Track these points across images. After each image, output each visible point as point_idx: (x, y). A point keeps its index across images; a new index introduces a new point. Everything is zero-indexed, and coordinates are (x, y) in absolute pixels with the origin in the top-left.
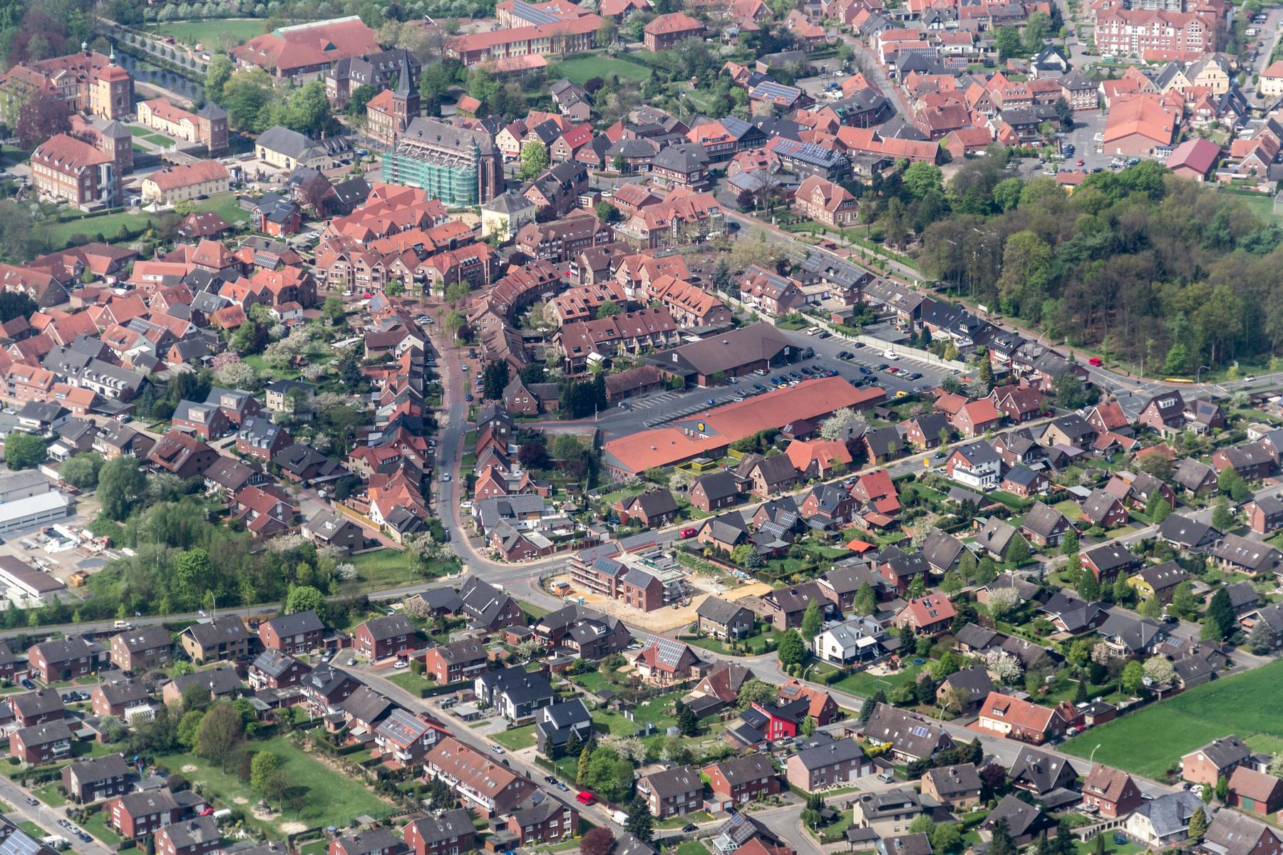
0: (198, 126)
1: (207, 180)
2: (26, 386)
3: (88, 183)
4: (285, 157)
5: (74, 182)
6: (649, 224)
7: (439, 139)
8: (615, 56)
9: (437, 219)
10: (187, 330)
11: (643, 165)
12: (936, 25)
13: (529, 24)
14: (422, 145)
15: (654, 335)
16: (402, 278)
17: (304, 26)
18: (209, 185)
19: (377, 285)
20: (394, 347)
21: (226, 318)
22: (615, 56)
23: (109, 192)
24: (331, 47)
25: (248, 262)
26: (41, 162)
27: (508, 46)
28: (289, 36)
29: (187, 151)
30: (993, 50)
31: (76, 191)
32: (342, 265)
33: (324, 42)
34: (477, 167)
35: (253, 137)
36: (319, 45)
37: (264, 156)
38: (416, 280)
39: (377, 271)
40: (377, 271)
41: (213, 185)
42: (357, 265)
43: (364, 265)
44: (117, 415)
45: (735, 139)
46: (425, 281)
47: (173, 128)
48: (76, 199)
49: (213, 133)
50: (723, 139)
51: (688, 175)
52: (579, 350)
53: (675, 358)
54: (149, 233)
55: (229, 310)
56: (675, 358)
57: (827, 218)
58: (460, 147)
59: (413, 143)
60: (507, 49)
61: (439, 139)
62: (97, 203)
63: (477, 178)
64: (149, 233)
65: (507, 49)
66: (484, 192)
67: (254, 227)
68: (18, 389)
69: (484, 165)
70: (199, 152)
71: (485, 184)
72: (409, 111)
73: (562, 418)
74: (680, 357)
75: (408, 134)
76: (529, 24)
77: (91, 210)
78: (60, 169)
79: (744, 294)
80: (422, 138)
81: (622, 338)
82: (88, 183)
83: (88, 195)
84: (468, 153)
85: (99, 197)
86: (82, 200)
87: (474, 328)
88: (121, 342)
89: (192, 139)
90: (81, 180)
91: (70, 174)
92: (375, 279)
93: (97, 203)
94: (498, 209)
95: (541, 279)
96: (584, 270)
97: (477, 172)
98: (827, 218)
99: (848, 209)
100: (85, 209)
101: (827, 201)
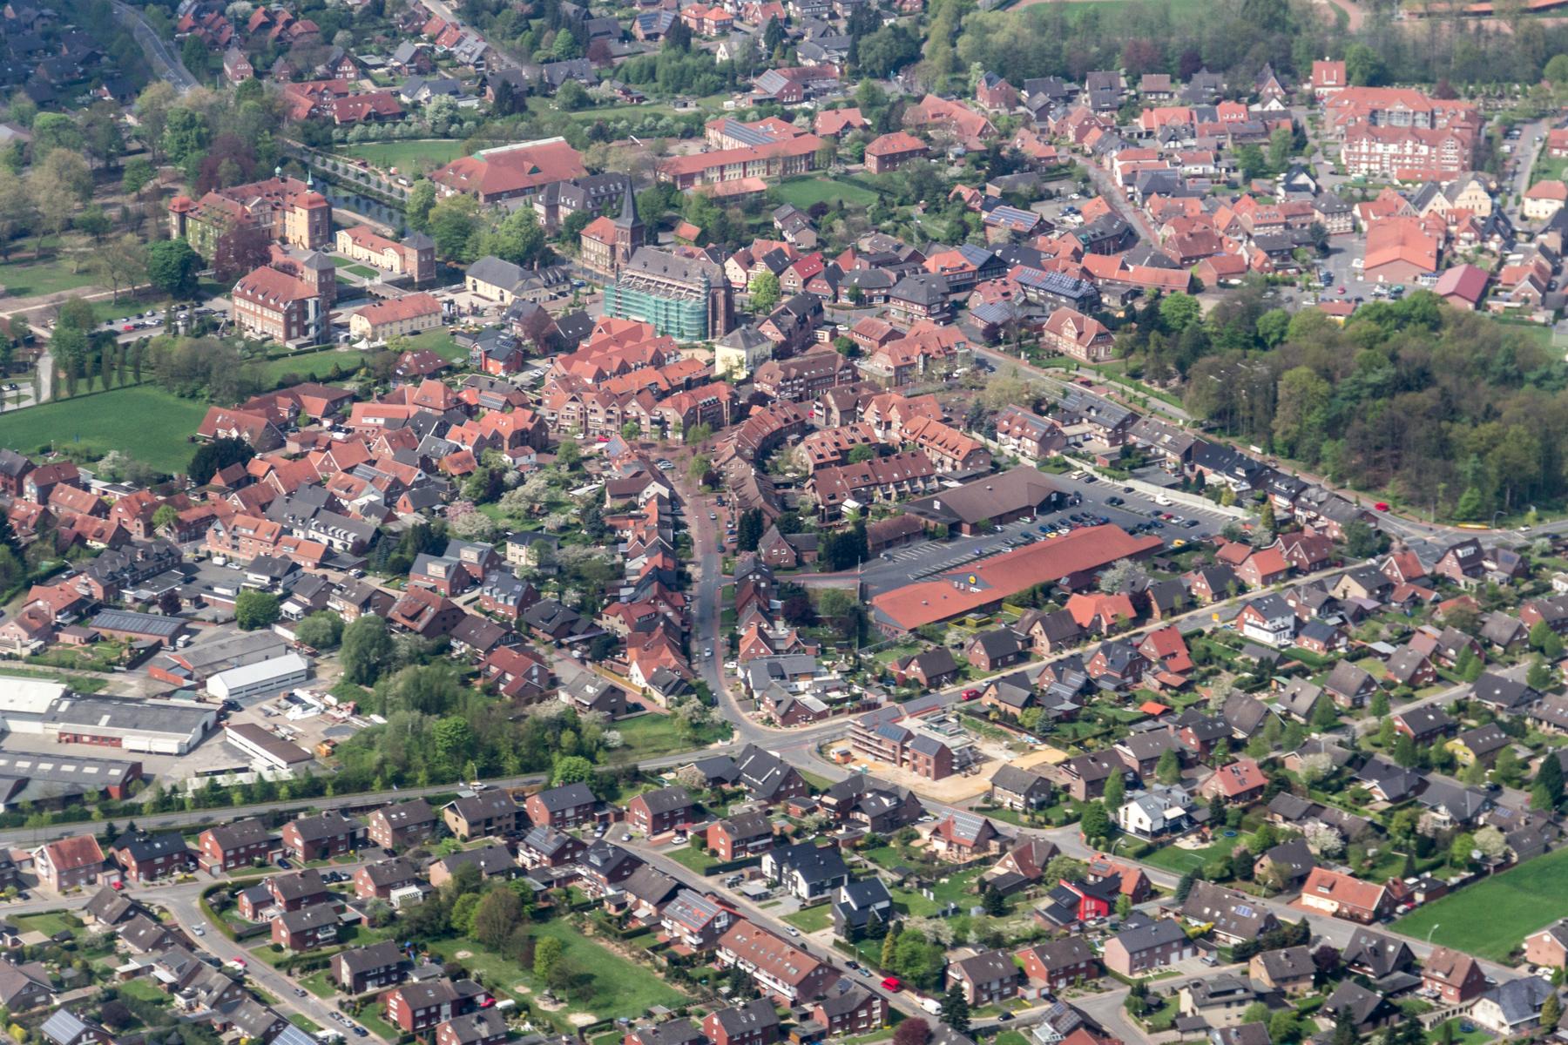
0: (403, 256)
1: (420, 315)
2: (251, 538)
3: (294, 318)
5: (280, 318)
6: (894, 361)
8: (835, 178)
10: (415, 478)
11: (879, 297)
12: (1172, 144)
13: (743, 145)
15: (912, 481)
16: (638, 420)
17: (517, 147)
18: (421, 320)
19: (611, 427)
20: (637, 495)
21: (456, 463)
22: (835, 178)
23: (317, 328)
24: (535, 170)
25: (473, 403)
26: (243, 296)
27: (722, 168)
28: (490, 158)
29: (391, 283)
30: (1235, 170)
31: (282, 327)
32: (573, 406)
33: (528, 166)
35: (461, 267)
36: (523, 168)
37: (475, 288)
38: (653, 422)
39: (610, 412)
40: (610, 412)
41: (425, 319)
42: (591, 406)
43: (597, 406)
44: (349, 569)
45: (975, 268)
46: (662, 423)
47: (376, 258)
48: (281, 335)
49: (420, 264)
50: (962, 268)
51: (929, 307)
52: (833, 497)
53: (937, 505)
54: (363, 371)
55: (458, 455)
56: (937, 505)
57: (1080, 353)
58: (688, 279)
62: (304, 340)
64: (363, 371)
66: (714, 326)
67: (474, 365)
68: (242, 542)
70: (405, 284)
71: (715, 318)
73: (822, 571)
74: (942, 505)
75: (631, 265)
76: (743, 145)
77: (298, 347)
78: (265, 304)
79: (999, 435)
81: (878, 484)
82: (294, 318)
83: (294, 331)
84: (697, 285)
85: (306, 334)
86: (288, 337)
87: (720, 474)
88: (348, 490)
89: (397, 270)
90: (288, 315)
91: (275, 309)
92: (609, 421)
93: (304, 340)
94: (733, 345)
95: (786, 420)
96: (829, 410)
98: (1080, 353)
99: (1102, 343)
100: (291, 346)
101: (1080, 334)
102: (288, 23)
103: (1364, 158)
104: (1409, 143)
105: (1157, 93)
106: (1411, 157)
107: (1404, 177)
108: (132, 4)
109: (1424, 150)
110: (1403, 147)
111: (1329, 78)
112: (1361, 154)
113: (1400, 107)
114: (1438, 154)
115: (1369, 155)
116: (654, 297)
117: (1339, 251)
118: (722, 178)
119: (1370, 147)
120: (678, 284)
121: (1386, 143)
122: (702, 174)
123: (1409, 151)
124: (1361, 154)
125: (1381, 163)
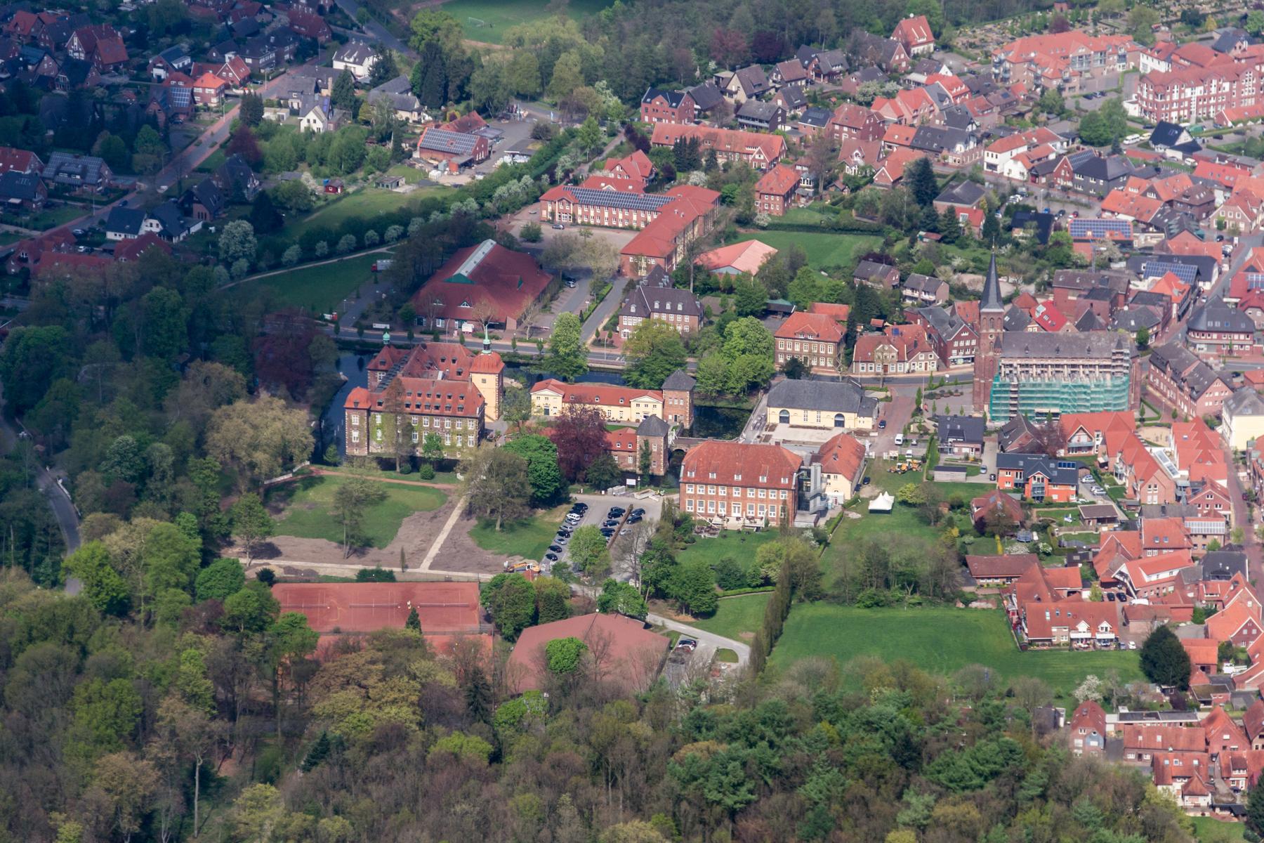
4: (834, 414)
7: (1058, 350)
80: (1060, 355)
91: (773, 485)
102: (586, 162)
103: (1175, 106)
104: (1214, 82)
105: (796, 80)
106: (1216, 96)
107: (1235, 118)
108: (995, 15)
109: (1227, 85)
110: (1207, 89)
111: (921, 36)
112: (1172, 102)
113: (1082, 51)
114: (1240, 87)
115: (1180, 102)
117: (331, 111)
119: (1181, 92)
121: (1193, 87)
123: (1213, 90)
124: (1172, 102)
125: (1189, 108)
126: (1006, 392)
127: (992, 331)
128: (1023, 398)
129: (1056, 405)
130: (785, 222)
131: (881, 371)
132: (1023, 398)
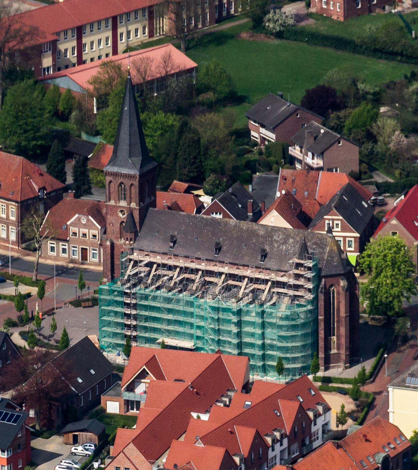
7: (218, 249)
8: (279, 35)
9: (317, 415)
14: (181, 263)
22: (279, 35)
27: (80, 32)
34: (316, 299)
58: (270, 263)
59: (158, 259)
60: (79, 39)
61: (218, 249)
63: (316, 321)
65: (79, 39)
66: (328, 348)
69: (327, 294)
71: (329, 332)
72: (141, 199)
75: (144, 243)
80: (177, 250)
97: (314, 312)
116: (208, 301)
118: (80, 47)
120: (248, 273)
122: (54, 44)
126: (170, 311)
127: (123, 203)
128: (147, 319)
129: (191, 336)
130: (344, 35)
131: (77, 257)
132: (147, 319)
